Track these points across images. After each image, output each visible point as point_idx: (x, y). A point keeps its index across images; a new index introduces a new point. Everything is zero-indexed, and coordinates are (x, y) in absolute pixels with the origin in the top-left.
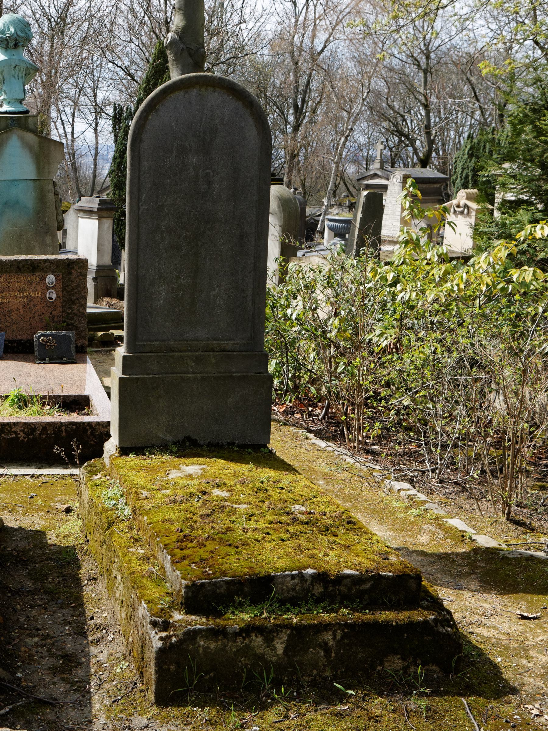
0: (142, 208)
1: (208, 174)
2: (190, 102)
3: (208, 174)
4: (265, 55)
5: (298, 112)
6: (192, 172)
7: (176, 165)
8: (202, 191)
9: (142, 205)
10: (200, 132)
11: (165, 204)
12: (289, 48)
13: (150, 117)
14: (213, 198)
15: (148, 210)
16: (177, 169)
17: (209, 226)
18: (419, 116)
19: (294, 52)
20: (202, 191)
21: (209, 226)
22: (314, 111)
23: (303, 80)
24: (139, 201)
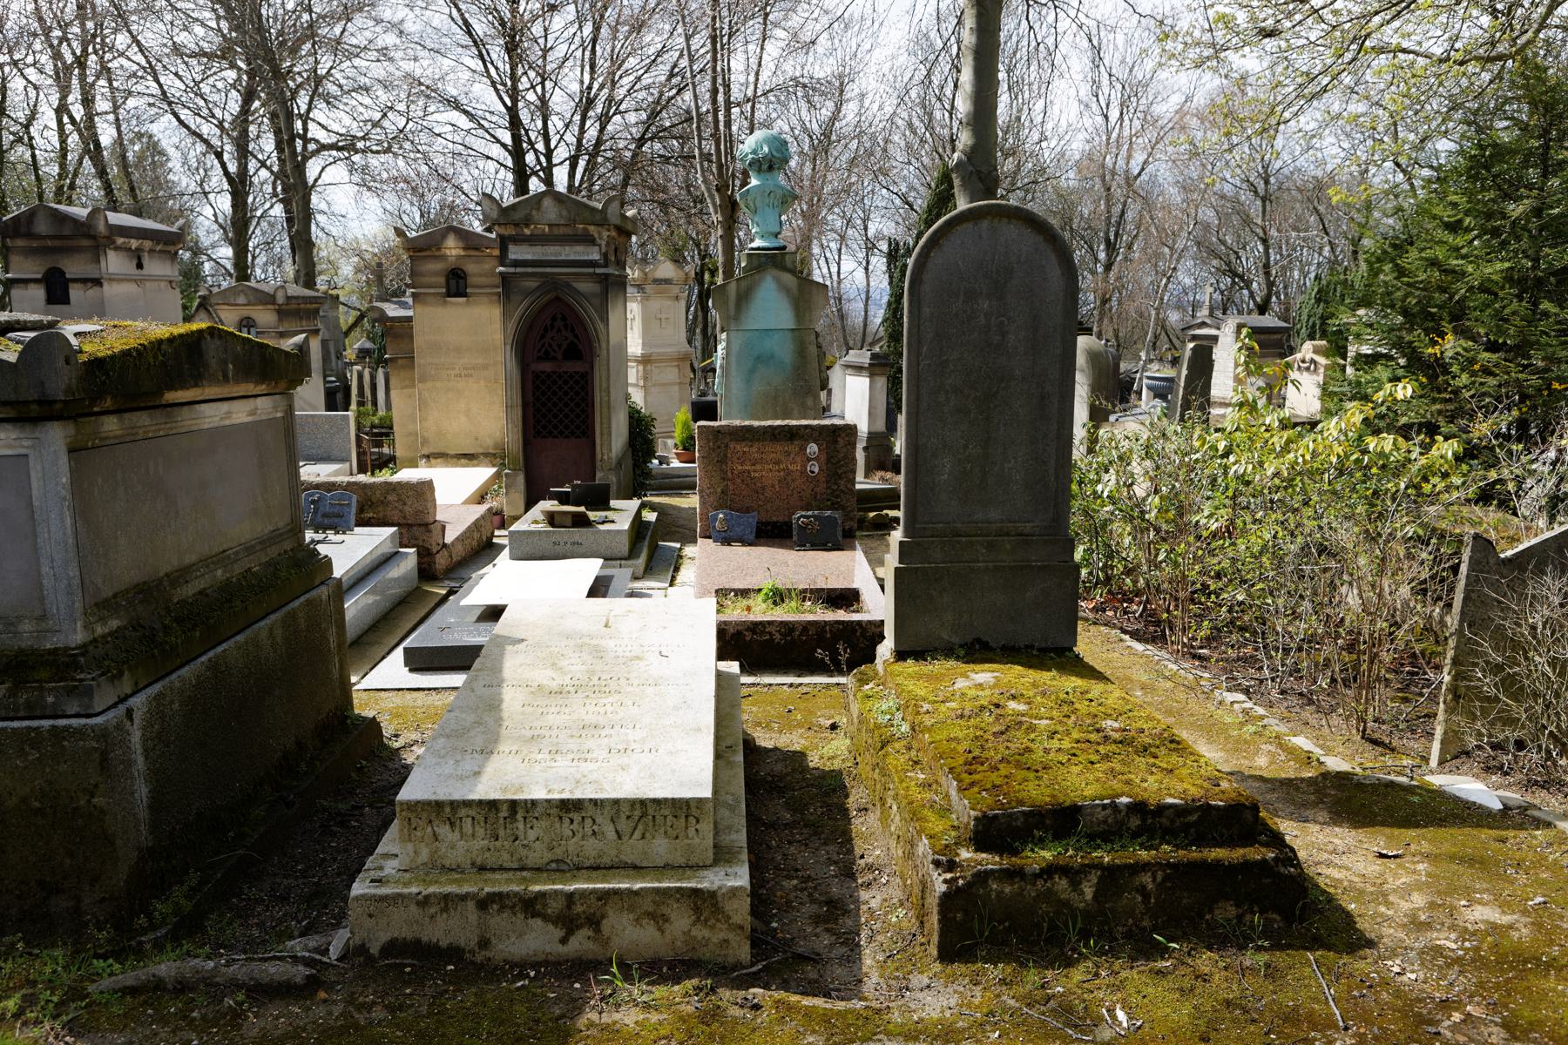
4: (1070, 179)
5: (1111, 247)
6: (982, 320)
12: (1099, 171)
19: (1105, 176)
22: (1130, 247)
23: (1116, 210)
24: (919, 354)
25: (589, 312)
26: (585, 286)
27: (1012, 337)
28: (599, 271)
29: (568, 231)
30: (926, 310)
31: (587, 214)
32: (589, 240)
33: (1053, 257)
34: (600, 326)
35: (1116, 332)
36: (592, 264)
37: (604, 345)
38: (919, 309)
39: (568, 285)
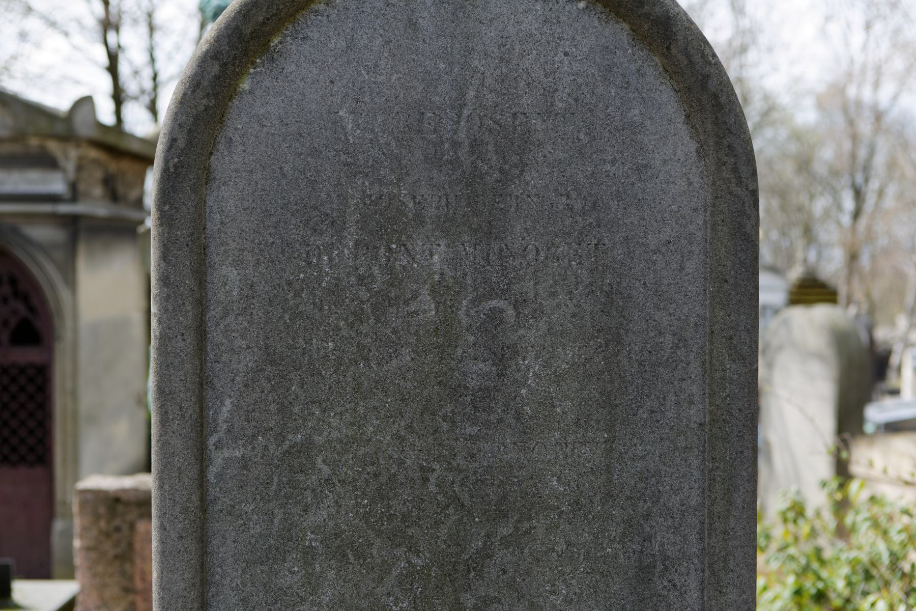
0: (218, 459)
1: (495, 316)
2: (412, 24)
3: (495, 316)
4: (807, 116)
5: (858, 195)
6: (427, 308)
7: (361, 279)
8: (472, 383)
9: (218, 446)
10: (456, 145)
11: (319, 439)
12: (838, 101)
13: (245, 85)
14: (518, 417)
15: (245, 464)
16: (365, 295)
17: (505, 530)
18: (279, 513)
19: (850, 112)
20: (472, 383)
21: (505, 530)
22: (881, 193)
23: (862, 153)
24: (201, 427)
25: (46, 271)
26: (42, 233)
27: (530, 366)
28: (64, 209)
29: (16, 148)
30: (227, 277)
31: (43, 124)
32: (48, 162)
33: (665, 96)
34: (64, 293)
35: (868, 295)
36: (53, 198)
37: (69, 323)
38: (201, 273)
39: (15, 231)
